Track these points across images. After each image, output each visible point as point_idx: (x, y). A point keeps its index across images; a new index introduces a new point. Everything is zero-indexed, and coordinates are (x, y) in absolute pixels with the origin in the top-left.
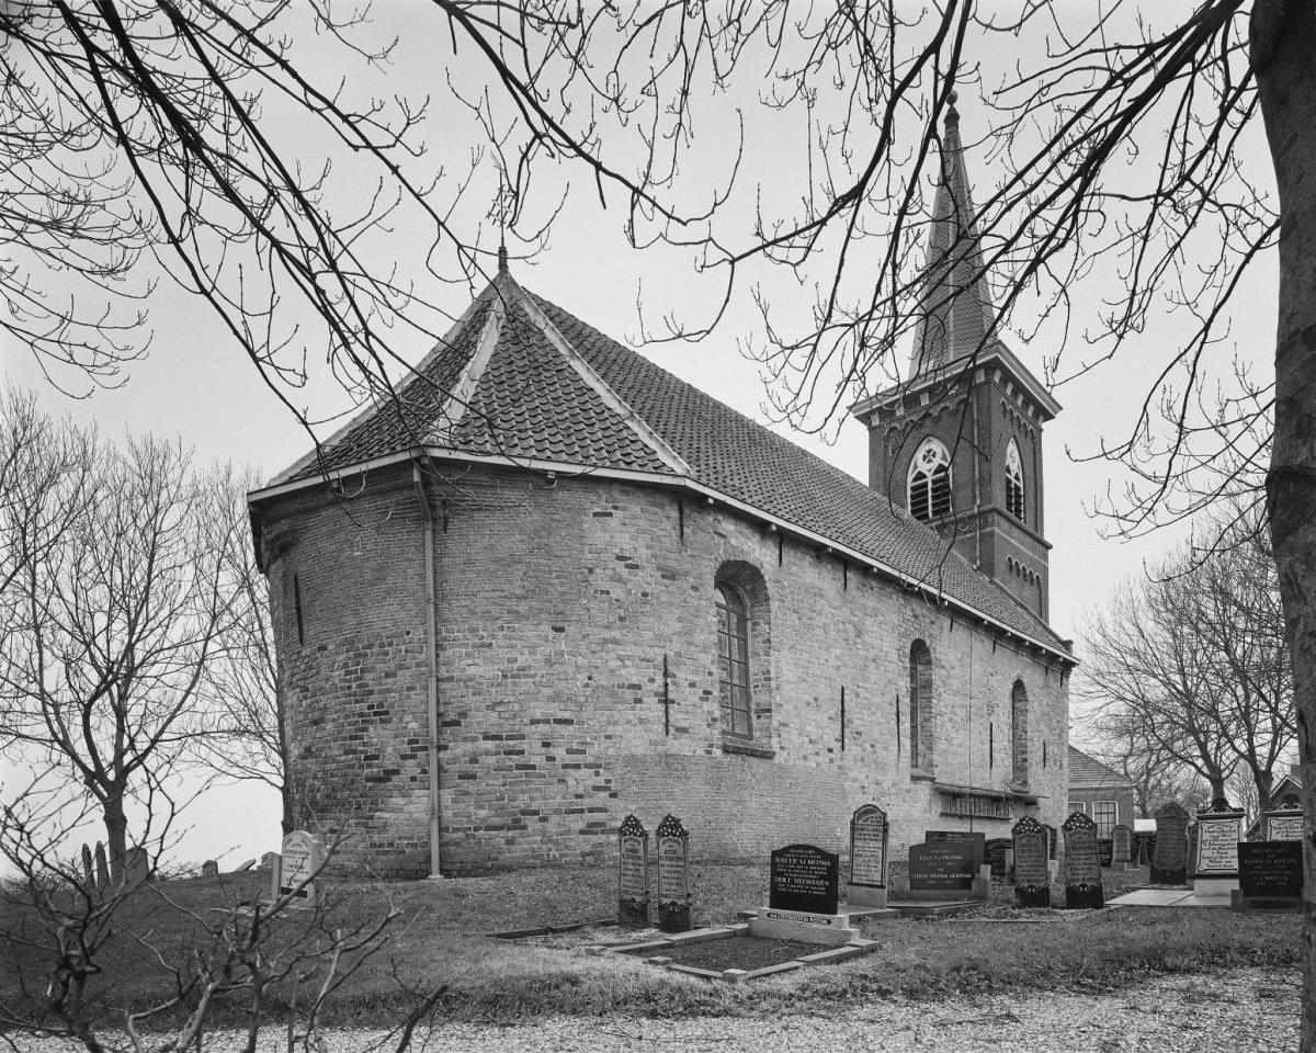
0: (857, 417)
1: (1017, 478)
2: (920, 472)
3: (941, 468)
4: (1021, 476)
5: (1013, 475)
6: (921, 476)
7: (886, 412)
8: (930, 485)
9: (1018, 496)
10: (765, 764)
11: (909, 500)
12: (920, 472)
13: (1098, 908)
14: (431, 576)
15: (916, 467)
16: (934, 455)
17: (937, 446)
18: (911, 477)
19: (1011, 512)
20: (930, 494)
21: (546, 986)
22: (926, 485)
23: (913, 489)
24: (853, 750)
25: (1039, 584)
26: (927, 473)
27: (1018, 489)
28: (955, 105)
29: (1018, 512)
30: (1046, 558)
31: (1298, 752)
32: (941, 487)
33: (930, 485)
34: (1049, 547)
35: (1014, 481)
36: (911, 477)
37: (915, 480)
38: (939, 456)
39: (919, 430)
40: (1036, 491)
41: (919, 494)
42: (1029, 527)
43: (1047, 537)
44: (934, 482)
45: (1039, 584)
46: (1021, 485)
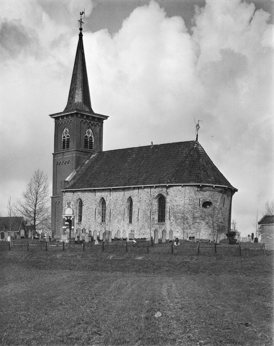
6: (64, 137)
18: (62, 137)
22: (65, 140)
36: (62, 137)
41: (64, 142)
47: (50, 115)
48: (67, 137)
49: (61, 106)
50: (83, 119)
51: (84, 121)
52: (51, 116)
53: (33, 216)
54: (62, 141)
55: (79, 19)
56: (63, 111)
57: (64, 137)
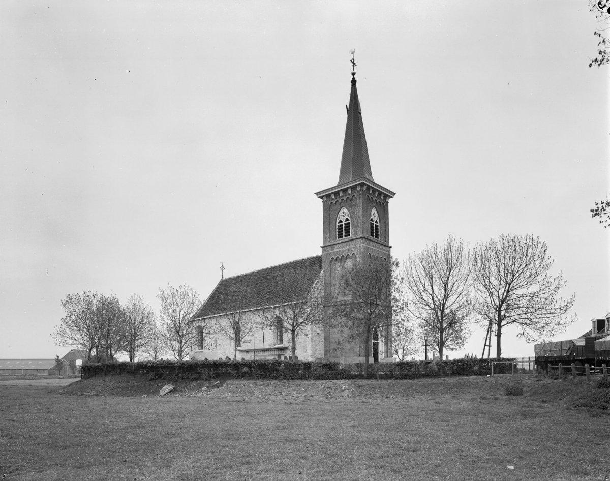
1: (376, 222)
2: (340, 220)
3: (347, 220)
5: (375, 221)
6: (341, 221)
7: (328, 196)
8: (344, 226)
9: (377, 229)
10: (202, 353)
11: (337, 233)
12: (340, 220)
13: (604, 326)
17: (345, 210)
18: (337, 222)
19: (373, 236)
20: (344, 231)
22: (342, 225)
23: (338, 226)
24: (218, 347)
27: (377, 226)
28: (355, 76)
29: (377, 237)
30: (389, 251)
32: (347, 225)
33: (344, 226)
34: (390, 247)
35: (375, 223)
36: (337, 222)
37: (339, 222)
38: (347, 215)
39: (342, 204)
41: (340, 227)
42: (382, 241)
43: (390, 245)
44: (345, 224)
46: (379, 225)
47: (315, 193)
48: (346, 221)
49: (331, 178)
50: (331, 201)
51: (334, 203)
52: (317, 195)
53: (290, 328)
54: (337, 227)
55: (355, 67)
56: (336, 185)
57: (341, 221)
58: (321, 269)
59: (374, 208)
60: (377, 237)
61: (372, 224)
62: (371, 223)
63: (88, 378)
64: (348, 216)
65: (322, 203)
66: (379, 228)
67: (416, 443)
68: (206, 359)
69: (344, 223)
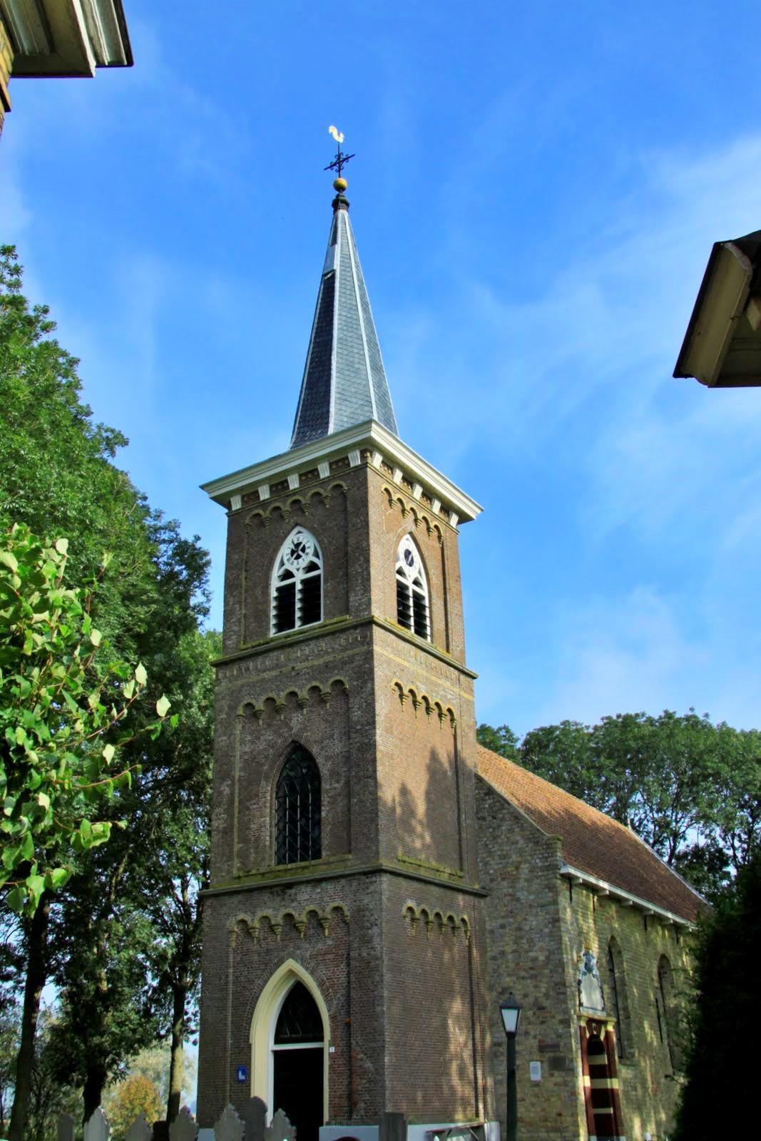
0: (215, 499)
3: (312, 567)
4: (423, 581)
6: (288, 575)
7: (250, 494)
9: (419, 606)
14: (339, 458)
15: (282, 564)
16: (303, 550)
21: (586, 939)
23: (279, 590)
25: (452, 720)
26: (295, 572)
27: (418, 598)
29: (420, 630)
31: (518, 1103)
32: (311, 586)
33: (299, 586)
35: (412, 587)
38: (310, 551)
40: (291, 645)
41: (286, 594)
44: (303, 582)
45: (452, 720)
46: (424, 592)
47: (202, 487)
57: (288, 575)
58: (324, 929)
59: (503, 1011)
60: (420, 630)
61: (401, 589)
62: (399, 583)
63: (561, 985)
64: (316, 555)
65: (226, 519)
66: (427, 603)
67: (343, 651)
68: (724, 724)
69: (299, 577)
